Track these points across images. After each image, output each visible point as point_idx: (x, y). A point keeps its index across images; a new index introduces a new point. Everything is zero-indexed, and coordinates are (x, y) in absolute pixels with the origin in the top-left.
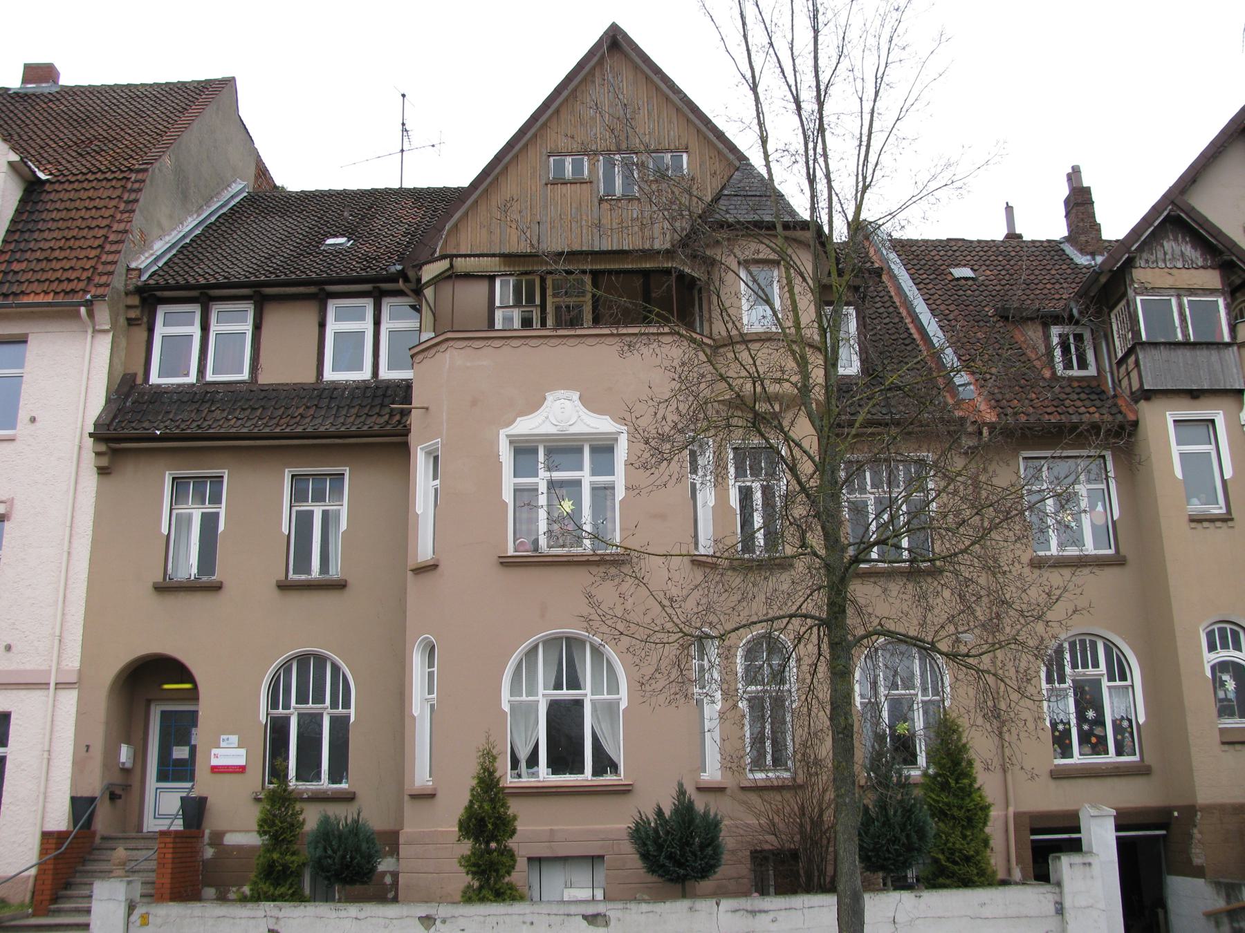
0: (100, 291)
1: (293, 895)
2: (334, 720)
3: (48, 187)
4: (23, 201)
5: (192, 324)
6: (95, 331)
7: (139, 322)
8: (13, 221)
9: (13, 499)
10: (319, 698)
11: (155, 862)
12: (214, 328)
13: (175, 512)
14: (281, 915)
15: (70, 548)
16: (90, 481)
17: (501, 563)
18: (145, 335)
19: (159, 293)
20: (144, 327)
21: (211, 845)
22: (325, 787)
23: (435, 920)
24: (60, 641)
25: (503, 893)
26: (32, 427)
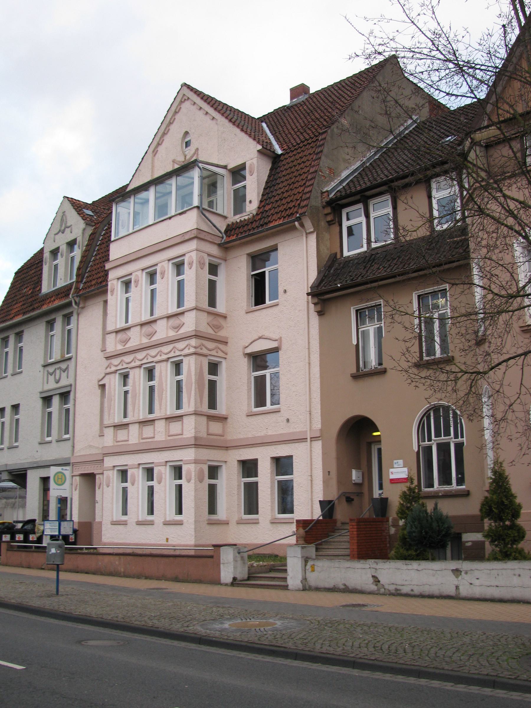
0: (304, 210)
1: (417, 555)
2: (439, 446)
3: (282, 158)
4: (271, 170)
5: (361, 216)
6: (307, 234)
7: (334, 222)
8: (267, 183)
9: (281, 337)
10: (447, 433)
11: (348, 537)
12: (373, 215)
13: (360, 330)
14: (377, 567)
15: (309, 360)
16: (315, 319)
17: (522, 331)
18: (338, 228)
19: (339, 202)
20: (337, 224)
21: (393, 526)
22: (454, 488)
23: (461, 571)
24: (310, 414)
25: (510, 555)
26: (285, 296)
